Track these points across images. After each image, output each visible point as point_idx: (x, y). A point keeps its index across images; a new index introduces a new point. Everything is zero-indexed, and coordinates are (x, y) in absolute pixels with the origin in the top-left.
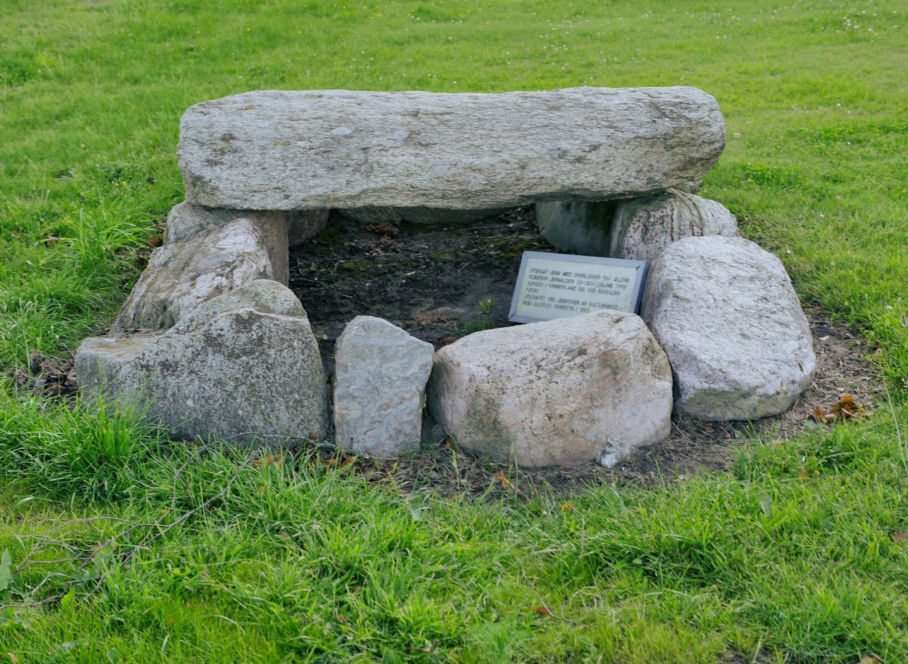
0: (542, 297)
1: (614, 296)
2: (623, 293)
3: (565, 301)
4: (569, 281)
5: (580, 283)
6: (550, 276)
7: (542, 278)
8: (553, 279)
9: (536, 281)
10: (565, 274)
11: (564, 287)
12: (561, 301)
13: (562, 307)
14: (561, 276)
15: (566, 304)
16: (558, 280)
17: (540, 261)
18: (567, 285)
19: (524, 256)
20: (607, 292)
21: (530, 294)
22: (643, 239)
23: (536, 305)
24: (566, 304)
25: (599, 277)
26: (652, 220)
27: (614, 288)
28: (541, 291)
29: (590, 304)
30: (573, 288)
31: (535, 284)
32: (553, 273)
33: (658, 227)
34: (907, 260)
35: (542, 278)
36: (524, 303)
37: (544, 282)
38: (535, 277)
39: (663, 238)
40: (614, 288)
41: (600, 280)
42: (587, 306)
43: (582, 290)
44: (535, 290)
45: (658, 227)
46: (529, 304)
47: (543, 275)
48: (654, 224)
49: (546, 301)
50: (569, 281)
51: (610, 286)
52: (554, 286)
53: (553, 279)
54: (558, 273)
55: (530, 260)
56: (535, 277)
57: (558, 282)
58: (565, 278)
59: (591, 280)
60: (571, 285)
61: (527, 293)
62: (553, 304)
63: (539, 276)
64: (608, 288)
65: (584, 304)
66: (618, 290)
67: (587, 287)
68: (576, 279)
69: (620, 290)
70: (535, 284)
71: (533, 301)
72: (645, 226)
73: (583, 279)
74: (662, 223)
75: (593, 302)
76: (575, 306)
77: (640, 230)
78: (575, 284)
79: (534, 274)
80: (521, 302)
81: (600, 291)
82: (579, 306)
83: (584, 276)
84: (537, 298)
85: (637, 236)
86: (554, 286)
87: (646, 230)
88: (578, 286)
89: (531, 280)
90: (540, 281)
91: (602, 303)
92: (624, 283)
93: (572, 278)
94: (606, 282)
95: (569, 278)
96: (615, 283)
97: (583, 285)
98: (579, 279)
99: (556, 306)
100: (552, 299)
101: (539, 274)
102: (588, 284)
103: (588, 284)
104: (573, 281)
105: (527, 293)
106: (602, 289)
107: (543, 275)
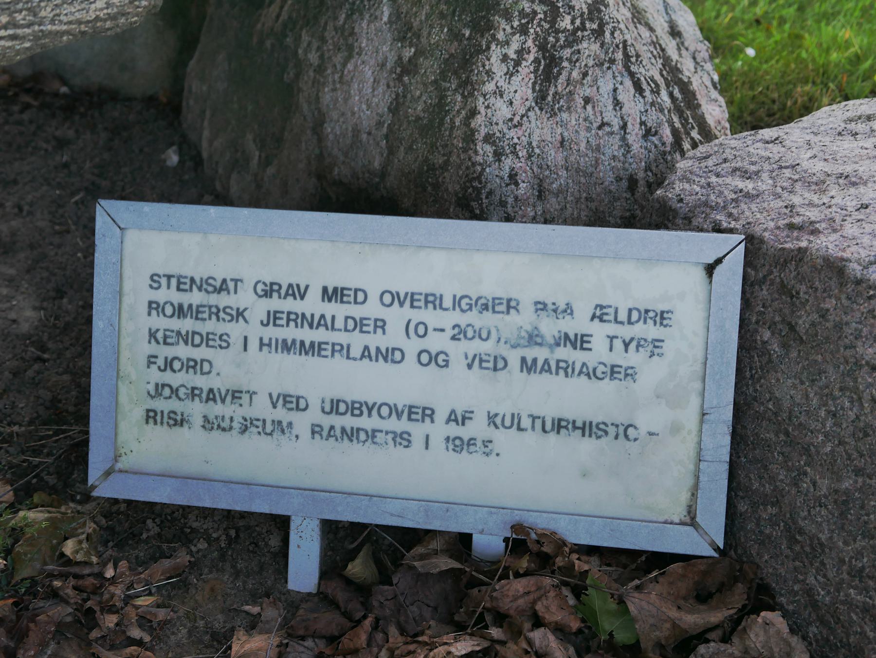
0: (235, 395)
1: (607, 386)
2: (651, 372)
3: (356, 408)
4: (360, 324)
5: (421, 330)
6: (259, 308)
7: (216, 313)
8: (273, 318)
9: (187, 325)
10: (333, 294)
11: (344, 350)
12: (334, 407)
13: (351, 435)
14: (312, 305)
15: (366, 422)
16: (294, 319)
17: (191, 241)
18: (357, 341)
19: (101, 221)
20: (565, 369)
21: (175, 379)
22: (541, 98)
23: (208, 424)
24: (366, 422)
25: (511, 305)
26: (566, 23)
27: (599, 352)
28: (226, 369)
29: (492, 419)
30: (388, 355)
31: (187, 338)
32: (270, 290)
33: (589, 48)
34: (2, 33)
35: (216, 313)
36: (151, 416)
37: (235, 330)
38: (180, 311)
39: (606, 85)
40: (599, 352)
41: (525, 319)
42: (477, 428)
43: (434, 360)
44: (193, 365)
45: (589, 48)
46: (178, 421)
47: (223, 300)
48: (573, 39)
49: (262, 408)
50: (360, 324)
51: (580, 342)
52: (287, 347)
53: (273, 318)
54: (297, 292)
55: (132, 236)
56: (180, 311)
57: (299, 322)
58: (336, 310)
59: (474, 318)
60: (375, 340)
61: (155, 376)
62: (302, 422)
63: (196, 306)
64: (565, 353)
65: (458, 418)
66: (618, 357)
67: (457, 351)
68: (397, 317)
69: (633, 358)
70: (187, 338)
71: (196, 409)
72: (542, 47)
73: (430, 317)
74: (599, 33)
75: (504, 409)
76: (418, 431)
77: (526, 67)
78: (394, 337)
79: (167, 295)
80: (132, 413)
81: (528, 366)
82: (439, 430)
83: (433, 301)
84: (211, 396)
85: (521, 87)
86: (287, 347)
87: (548, 68)
88: (412, 346)
89: (161, 323)
90: (210, 326)
91: (550, 412)
92: (650, 331)
93: (372, 309)
94: (549, 327)
95: (357, 311)
96: (599, 332)
97: (435, 343)
98: (407, 312)
99: (316, 430)
100: (292, 402)
101: (196, 298)
102: (459, 334)
103: (459, 334)
104: (380, 325)
105: (155, 376)
106: (541, 354)
107: (223, 300)
